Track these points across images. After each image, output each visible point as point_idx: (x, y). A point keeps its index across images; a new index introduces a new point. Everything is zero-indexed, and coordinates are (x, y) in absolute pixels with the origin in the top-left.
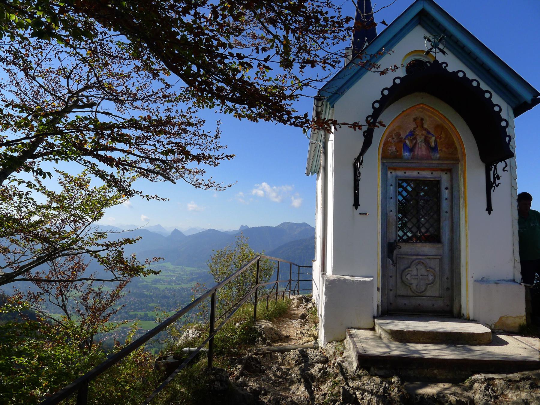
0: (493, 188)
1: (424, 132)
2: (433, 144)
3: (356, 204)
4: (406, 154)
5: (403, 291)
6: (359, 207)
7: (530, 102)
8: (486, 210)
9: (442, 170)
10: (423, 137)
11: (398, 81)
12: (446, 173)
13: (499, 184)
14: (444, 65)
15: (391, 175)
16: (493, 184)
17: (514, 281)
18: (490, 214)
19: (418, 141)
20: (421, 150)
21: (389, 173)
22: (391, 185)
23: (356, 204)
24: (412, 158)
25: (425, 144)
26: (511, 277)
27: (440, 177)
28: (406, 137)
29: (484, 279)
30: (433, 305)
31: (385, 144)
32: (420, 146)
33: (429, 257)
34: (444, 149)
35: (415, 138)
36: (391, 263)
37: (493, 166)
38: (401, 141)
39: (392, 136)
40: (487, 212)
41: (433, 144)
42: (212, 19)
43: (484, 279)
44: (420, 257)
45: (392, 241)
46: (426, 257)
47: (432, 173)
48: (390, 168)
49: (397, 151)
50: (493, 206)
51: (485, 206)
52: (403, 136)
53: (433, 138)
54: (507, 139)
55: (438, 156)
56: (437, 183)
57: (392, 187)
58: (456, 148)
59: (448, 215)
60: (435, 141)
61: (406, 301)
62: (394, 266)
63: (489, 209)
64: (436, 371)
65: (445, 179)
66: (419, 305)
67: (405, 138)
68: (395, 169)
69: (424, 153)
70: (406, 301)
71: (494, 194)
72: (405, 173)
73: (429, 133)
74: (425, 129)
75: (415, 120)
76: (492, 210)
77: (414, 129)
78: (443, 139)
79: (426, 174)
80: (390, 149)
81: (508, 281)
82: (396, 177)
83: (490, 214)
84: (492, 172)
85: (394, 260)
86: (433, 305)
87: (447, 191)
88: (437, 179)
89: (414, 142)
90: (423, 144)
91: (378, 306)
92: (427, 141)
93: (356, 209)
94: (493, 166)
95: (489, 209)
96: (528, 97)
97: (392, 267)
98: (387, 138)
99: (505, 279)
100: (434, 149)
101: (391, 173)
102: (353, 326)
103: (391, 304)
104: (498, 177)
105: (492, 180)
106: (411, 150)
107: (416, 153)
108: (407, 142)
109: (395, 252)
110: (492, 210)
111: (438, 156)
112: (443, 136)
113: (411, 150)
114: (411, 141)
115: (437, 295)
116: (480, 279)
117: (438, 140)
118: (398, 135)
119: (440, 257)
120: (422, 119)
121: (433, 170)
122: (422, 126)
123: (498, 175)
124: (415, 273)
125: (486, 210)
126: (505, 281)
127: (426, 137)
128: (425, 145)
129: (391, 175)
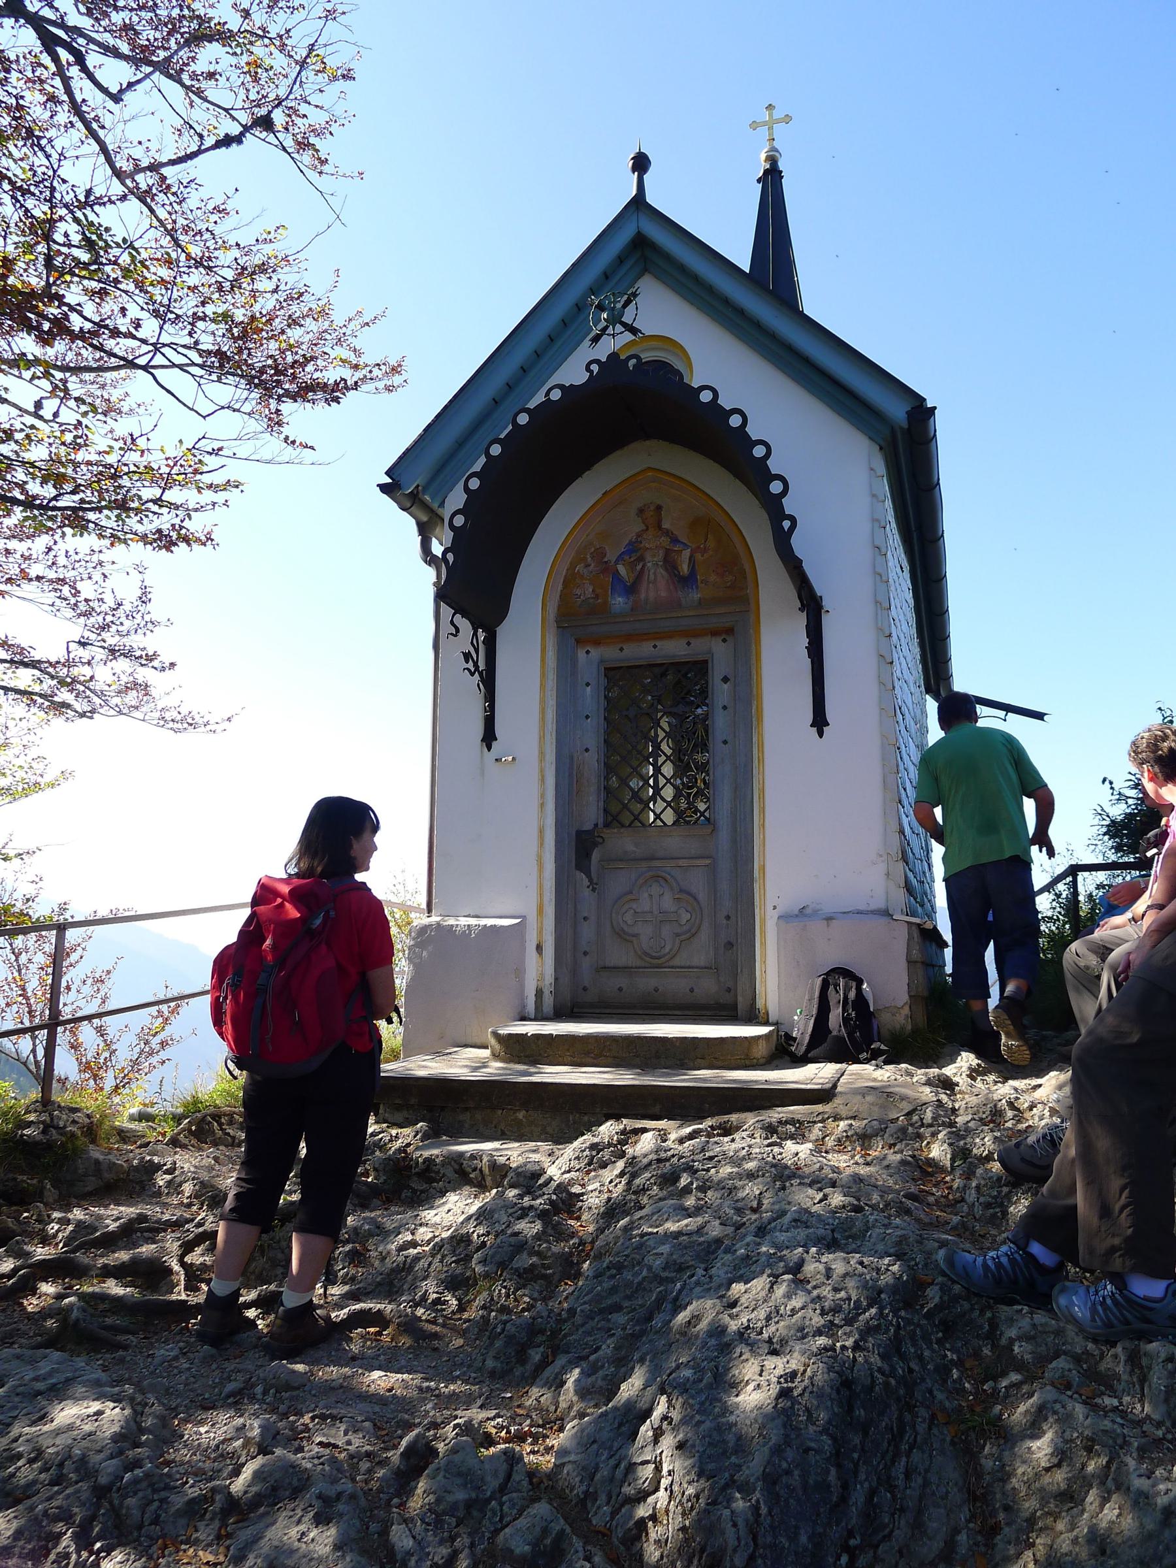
1: (665, 541)
2: (685, 569)
3: (489, 737)
4: (619, 602)
5: (618, 956)
8: (812, 726)
9: (715, 633)
10: (661, 553)
11: (735, 421)
12: (724, 641)
15: (589, 659)
17: (886, 913)
18: (821, 734)
19: (649, 565)
20: (656, 587)
21: (581, 654)
22: (588, 684)
23: (489, 737)
24: (632, 610)
25: (666, 570)
26: (879, 903)
27: (710, 652)
28: (620, 559)
29: (808, 911)
30: (692, 990)
31: (566, 583)
32: (652, 577)
33: (681, 863)
34: (713, 578)
35: (641, 559)
36: (586, 882)
38: (607, 569)
39: (585, 559)
41: (685, 569)
43: (808, 911)
44: (657, 863)
45: (588, 826)
46: (673, 863)
47: (689, 644)
48: (579, 642)
49: (597, 597)
50: (830, 715)
51: (809, 717)
52: (611, 556)
53: (686, 554)
55: (695, 596)
56: (701, 667)
57: (589, 689)
60: (691, 558)
61: (622, 981)
62: (594, 890)
63: (820, 722)
64: (521, 1115)
65: (720, 652)
66: (656, 990)
67: (617, 562)
68: (597, 643)
69: (663, 594)
70: (622, 981)
72: (621, 649)
73: (675, 540)
74: (667, 533)
75: (641, 511)
77: (639, 535)
78: (711, 553)
79: (674, 649)
80: (578, 592)
81: (873, 912)
82: (602, 661)
83: (821, 734)
85: (594, 875)
86: (692, 990)
87: (726, 686)
88: (700, 658)
89: (639, 567)
90: (661, 571)
91: (539, 993)
92: (670, 564)
93: (489, 748)
95: (820, 722)
97: (587, 892)
98: (572, 566)
99: (862, 907)
100: (688, 581)
101: (588, 652)
102: (469, 1042)
103: (585, 989)
106: (631, 589)
107: (643, 596)
108: (622, 569)
109: (596, 855)
111: (695, 596)
112: (711, 543)
113: (631, 589)
114: (631, 566)
115: (702, 964)
116: (796, 912)
117: (698, 556)
118: (599, 554)
119: (708, 861)
120: (659, 508)
121: (689, 634)
122: (659, 526)
124: (647, 908)
125: (812, 726)
126: (859, 912)
127: (668, 552)
128: (664, 573)
129: (589, 659)
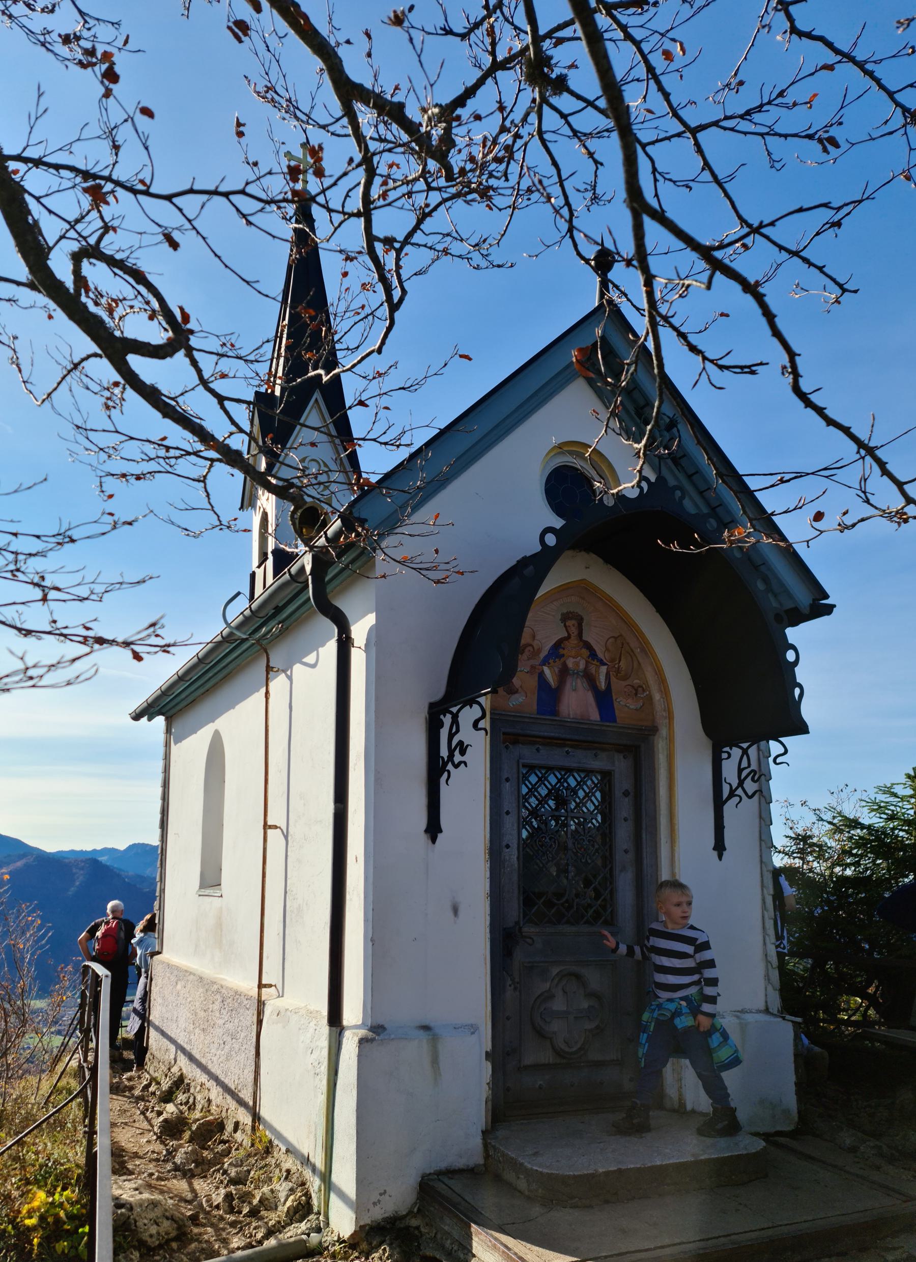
0: (446, 774)
6: (440, 835)
7: (806, 611)
13: (460, 763)
14: (678, 493)
16: (445, 764)
18: (720, 857)
37: (449, 716)
40: (715, 853)
42: (626, 367)
50: (727, 843)
53: (604, 669)
54: (797, 691)
58: (650, 698)
59: (631, 856)
71: (446, 792)
76: (441, 831)
83: (720, 857)
84: (444, 733)
87: (627, 799)
94: (449, 716)
96: (803, 598)
104: (463, 748)
105: (444, 752)
110: (441, 831)
123: (461, 743)
